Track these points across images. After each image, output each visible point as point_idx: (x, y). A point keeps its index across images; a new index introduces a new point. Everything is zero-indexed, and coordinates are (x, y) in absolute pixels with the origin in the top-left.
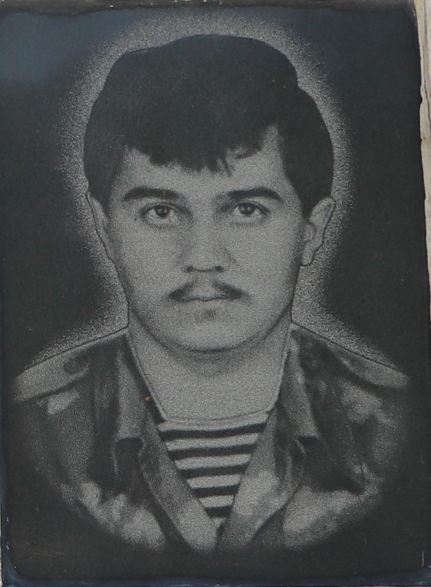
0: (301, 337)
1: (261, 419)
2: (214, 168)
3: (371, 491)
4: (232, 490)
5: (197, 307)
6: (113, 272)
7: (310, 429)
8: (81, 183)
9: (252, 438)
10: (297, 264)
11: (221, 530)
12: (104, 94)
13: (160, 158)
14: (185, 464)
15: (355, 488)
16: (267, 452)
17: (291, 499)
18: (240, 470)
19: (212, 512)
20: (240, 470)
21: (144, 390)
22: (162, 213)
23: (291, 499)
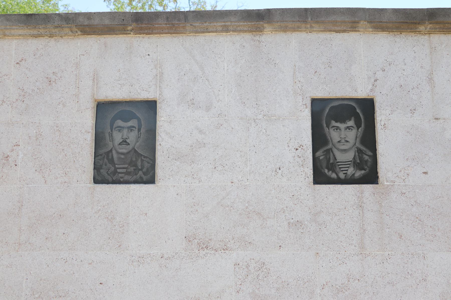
0: (357, 148)
1: (351, 160)
2: (344, 123)
3: (367, 170)
4: (347, 170)
5: (342, 143)
6: (330, 138)
7: (358, 161)
8: (325, 125)
9: (350, 163)
10: (357, 137)
11: (345, 176)
12: (328, 112)
13: (336, 122)
14: (340, 166)
15: (365, 170)
16: (352, 165)
17: (356, 172)
18: (348, 167)
19: (344, 173)
20: (348, 167)
21: (334, 156)
22: (337, 129)
23: (356, 172)
